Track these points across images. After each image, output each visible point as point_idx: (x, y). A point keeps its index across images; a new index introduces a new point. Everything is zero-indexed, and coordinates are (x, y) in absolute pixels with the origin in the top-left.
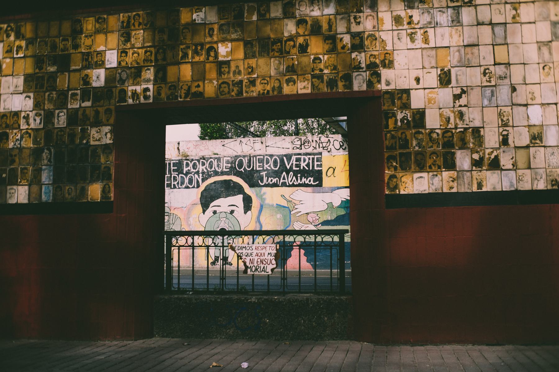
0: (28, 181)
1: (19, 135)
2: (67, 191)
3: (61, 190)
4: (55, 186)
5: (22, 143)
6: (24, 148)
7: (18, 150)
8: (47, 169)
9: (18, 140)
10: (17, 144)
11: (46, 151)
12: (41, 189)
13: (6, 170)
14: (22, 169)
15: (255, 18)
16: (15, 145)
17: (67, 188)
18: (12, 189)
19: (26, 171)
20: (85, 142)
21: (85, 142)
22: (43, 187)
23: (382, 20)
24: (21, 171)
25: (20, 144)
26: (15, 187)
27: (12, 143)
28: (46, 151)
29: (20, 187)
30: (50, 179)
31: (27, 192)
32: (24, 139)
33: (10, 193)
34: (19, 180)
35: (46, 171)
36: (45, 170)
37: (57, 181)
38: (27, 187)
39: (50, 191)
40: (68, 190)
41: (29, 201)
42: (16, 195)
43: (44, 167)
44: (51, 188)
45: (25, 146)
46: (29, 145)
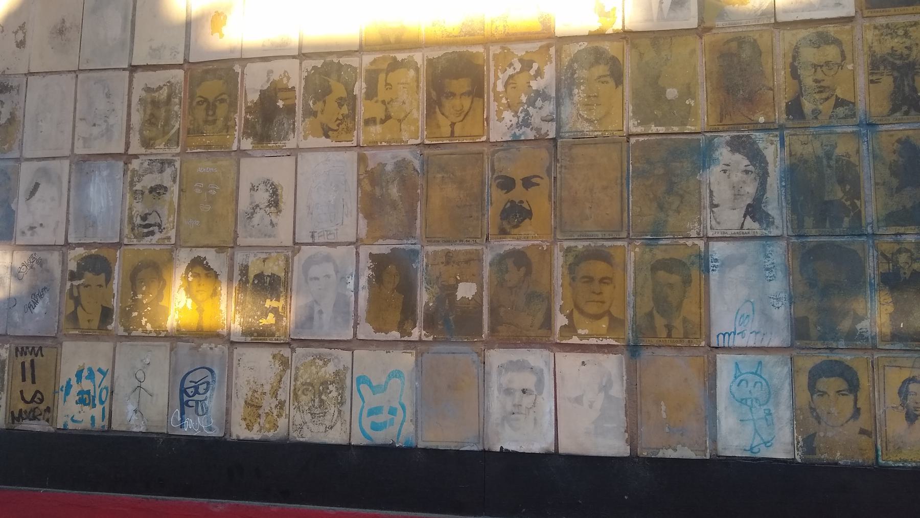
0: (616, 323)
1: (549, 71)
2: (892, 398)
3: (853, 387)
4: (808, 362)
5: (567, 111)
6: (580, 140)
7: (543, 154)
8: (742, 260)
9: (541, 95)
10: (536, 120)
11: (724, 154)
12: (710, 378)
13: (476, 258)
14: (576, 261)
15: (802, 198)
16: (526, 123)
17: (895, 378)
18: (520, 366)
19: (599, 269)
20: (848, 187)
21: (848, 187)
22: (725, 365)
23: (154, 51)
24: (572, 269)
25: (556, 119)
26: (536, 357)
27: (508, 115)
28: (724, 154)
29: (568, 362)
30: (767, 319)
31: (618, 391)
32: (579, 94)
33: (508, 392)
34: (561, 320)
35: (740, 271)
36: (727, 263)
37: (815, 334)
38: (612, 364)
39: (771, 393)
40: (903, 392)
41: (632, 441)
42: (548, 405)
43: (719, 250)
44: (777, 370)
45: (587, 128)
46: (612, 126)
